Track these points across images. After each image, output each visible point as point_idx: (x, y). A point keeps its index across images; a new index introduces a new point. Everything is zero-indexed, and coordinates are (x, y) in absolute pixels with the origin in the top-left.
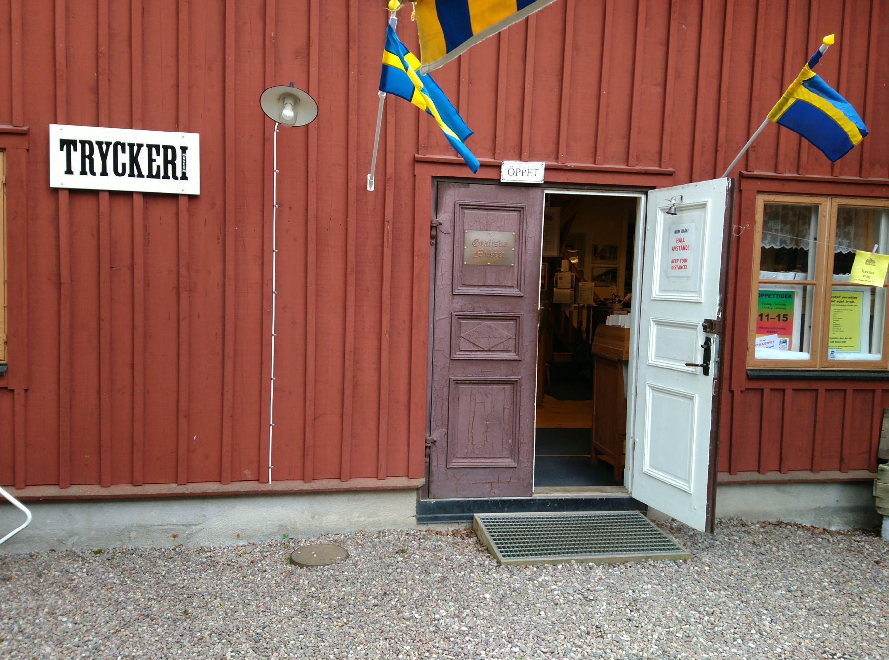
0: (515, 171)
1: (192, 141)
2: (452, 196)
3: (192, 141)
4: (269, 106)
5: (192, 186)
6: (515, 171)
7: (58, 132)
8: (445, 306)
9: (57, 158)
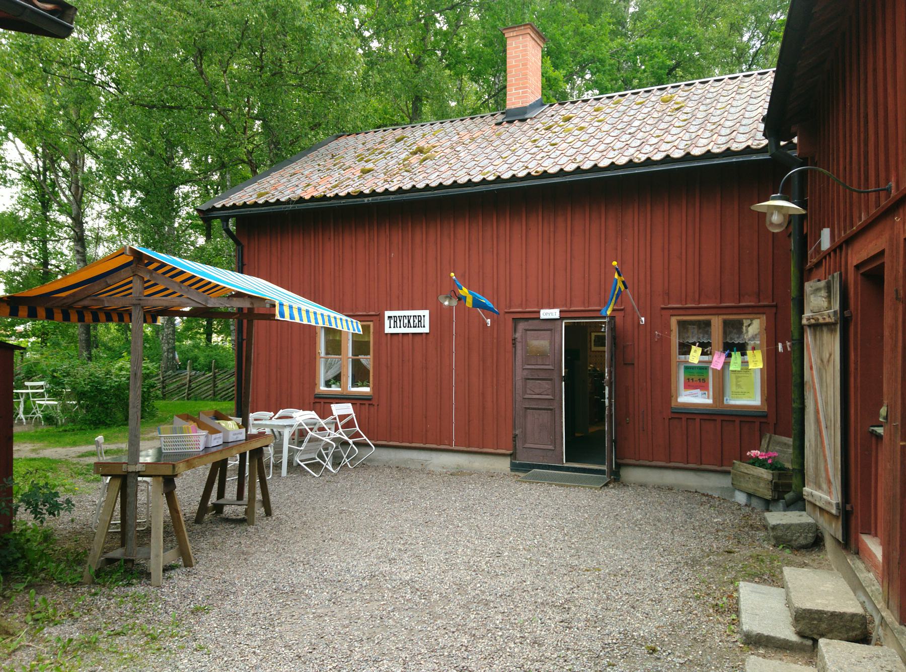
0: (547, 313)
1: (426, 313)
2: (522, 326)
3: (426, 313)
4: (441, 299)
5: (426, 330)
6: (547, 313)
7: (388, 313)
8: (520, 374)
9: (387, 322)
